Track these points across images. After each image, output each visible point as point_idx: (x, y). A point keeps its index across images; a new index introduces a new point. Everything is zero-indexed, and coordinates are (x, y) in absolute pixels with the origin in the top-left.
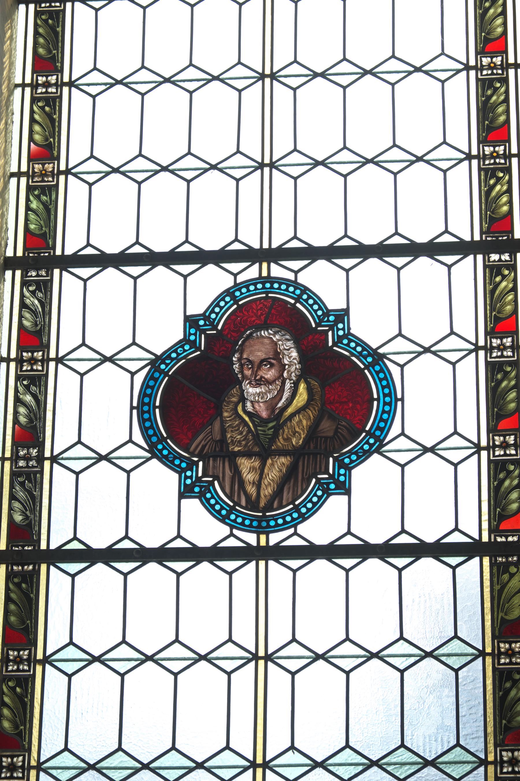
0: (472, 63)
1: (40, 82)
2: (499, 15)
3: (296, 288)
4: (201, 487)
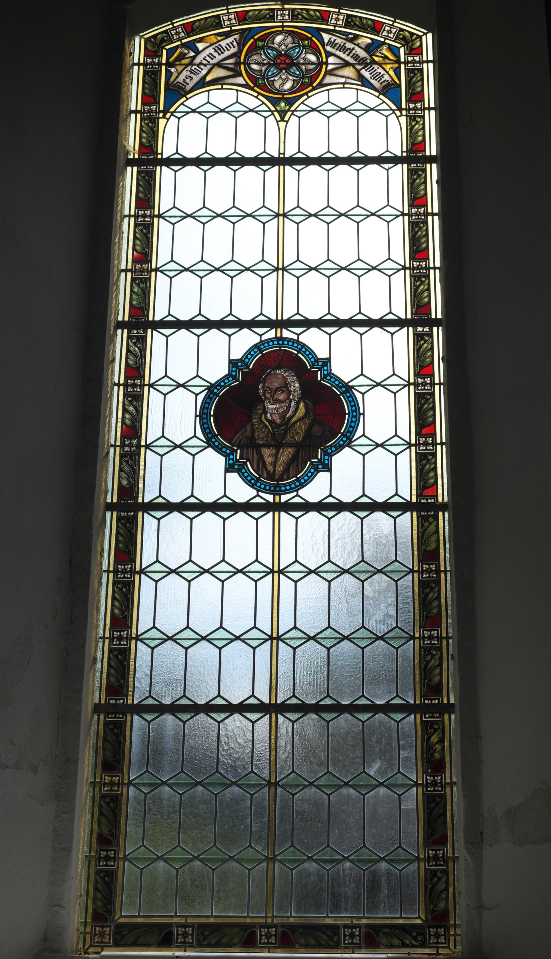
3: (298, 345)
4: (239, 465)
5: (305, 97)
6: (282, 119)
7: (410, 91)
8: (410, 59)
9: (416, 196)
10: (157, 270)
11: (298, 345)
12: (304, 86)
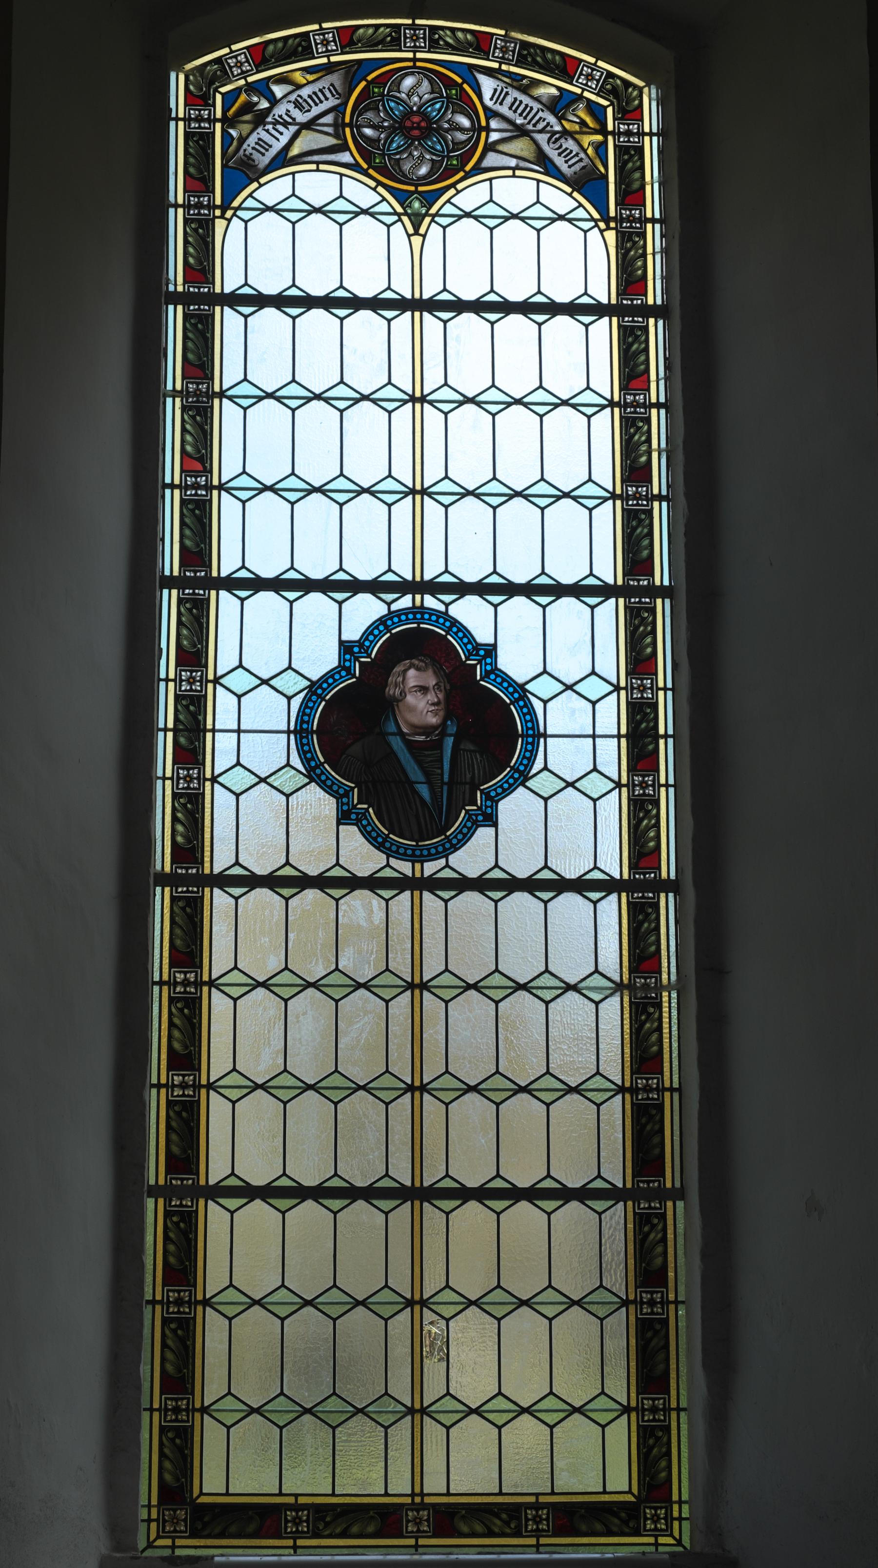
0: (618, 491)
1: (176, 1083)
2: (649, 634)
3: (446, 620)
5: (452, 191)
6: (416, 233)
7: (631, 555)
8: (623, 128)
9: (638, 657)
10: (222, 395)
11: (446, 620)
12: (450, 172)
